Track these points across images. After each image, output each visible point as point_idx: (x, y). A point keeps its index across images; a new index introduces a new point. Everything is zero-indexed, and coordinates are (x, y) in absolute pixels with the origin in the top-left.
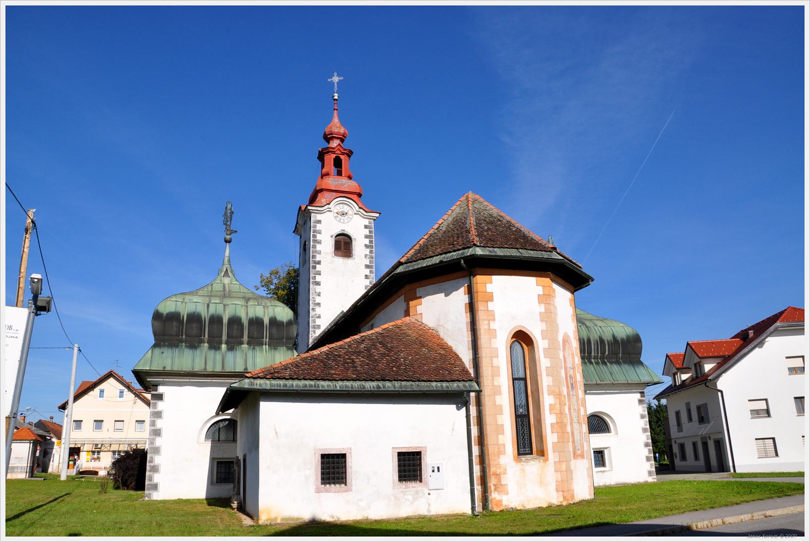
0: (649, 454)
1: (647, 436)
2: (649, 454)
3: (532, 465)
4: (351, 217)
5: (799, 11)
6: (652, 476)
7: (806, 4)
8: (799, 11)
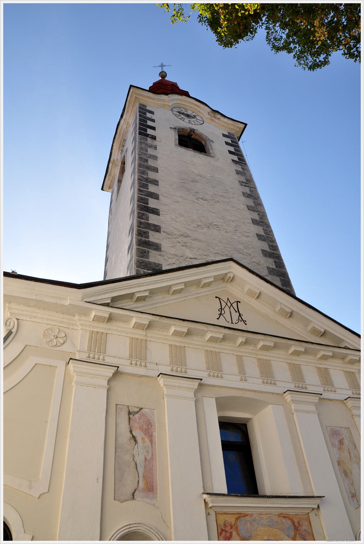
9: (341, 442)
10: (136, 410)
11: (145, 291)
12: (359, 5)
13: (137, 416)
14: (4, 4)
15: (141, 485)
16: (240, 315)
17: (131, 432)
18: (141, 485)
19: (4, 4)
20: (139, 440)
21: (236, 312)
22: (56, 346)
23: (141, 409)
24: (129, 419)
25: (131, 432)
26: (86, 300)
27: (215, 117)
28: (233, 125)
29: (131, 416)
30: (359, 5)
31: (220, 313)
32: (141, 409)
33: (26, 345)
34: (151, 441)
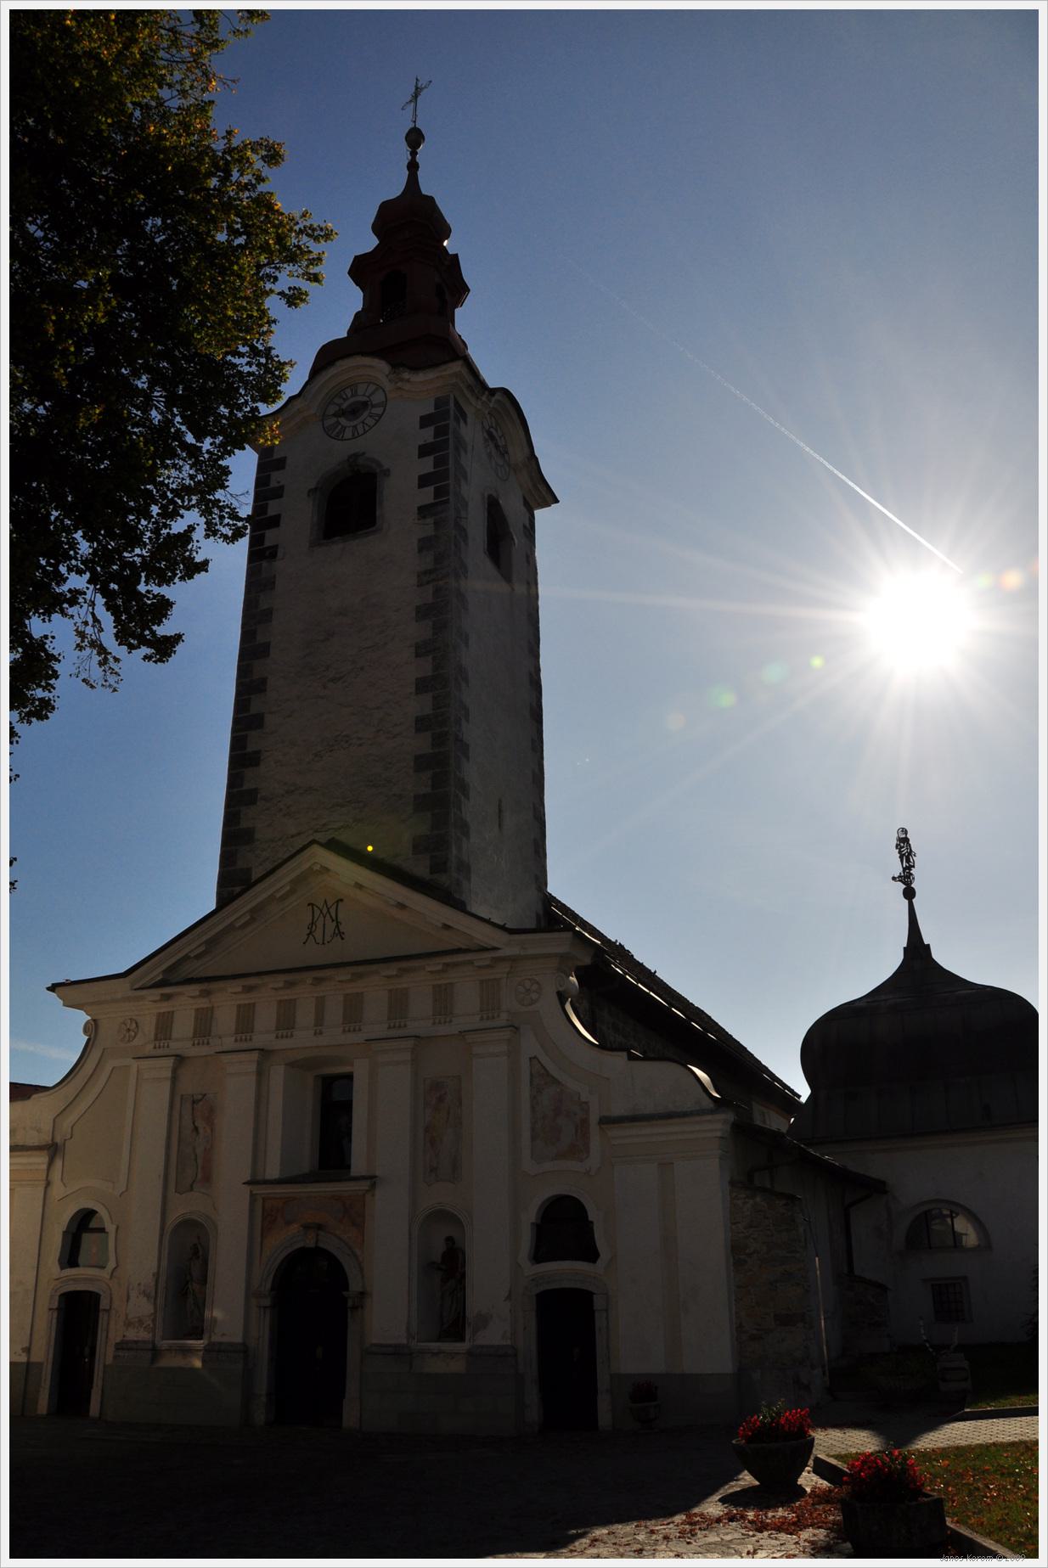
4: (379, 411)
5: (1029, 18)
7: (1041, 7)
8: (1029, 18)
9: (441, 1099)
10: (200, 1097)
11: (199, 946)
12: (1034, 1554)
13: (201, 1103)
14: (1036, 12)
15: (199, 1176)
16: (337, 926)
17: (194, 1123)
18: (199, 1176)
19: (1036, 12)
20: (201, 1131)
21: (333, 921)
22: (129, 1041)
23: (205, 1095)
24: (193, 1109)
25: (194, 1123)
26: (136, 987)
27: (402, 380)
28: (437, 377)
29: (195, 1105)
30: (1034, 1554)
31: (308, 931)
32: (205, 1095)
33: (104, 1049)
34: (212, 1130)
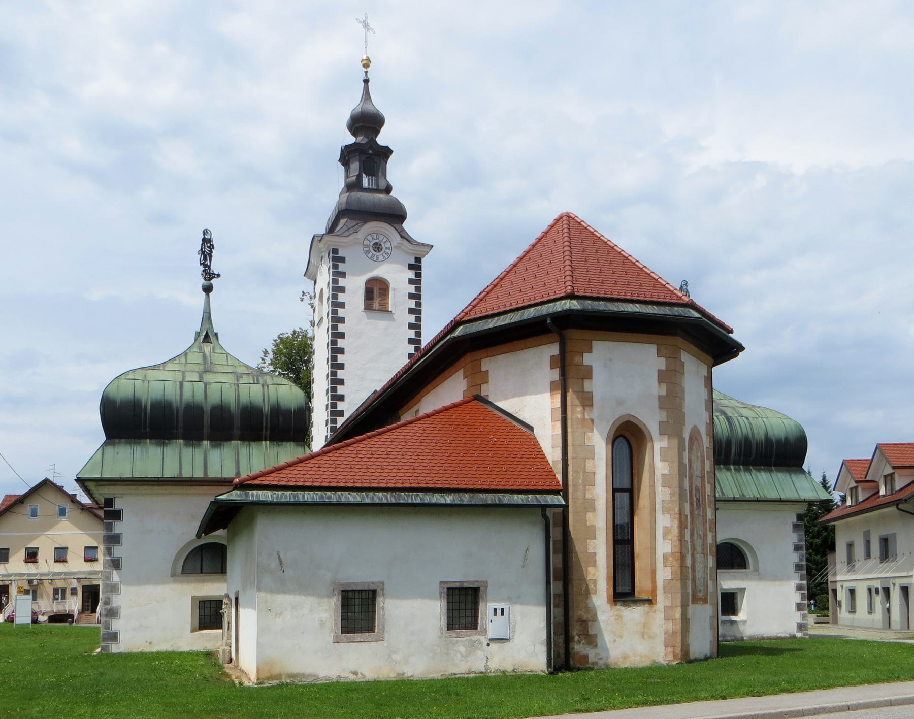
0: (802, 600)
1: (801, 575)
2: (802, 600)
3: (633, 614)
6: (802, 630)
